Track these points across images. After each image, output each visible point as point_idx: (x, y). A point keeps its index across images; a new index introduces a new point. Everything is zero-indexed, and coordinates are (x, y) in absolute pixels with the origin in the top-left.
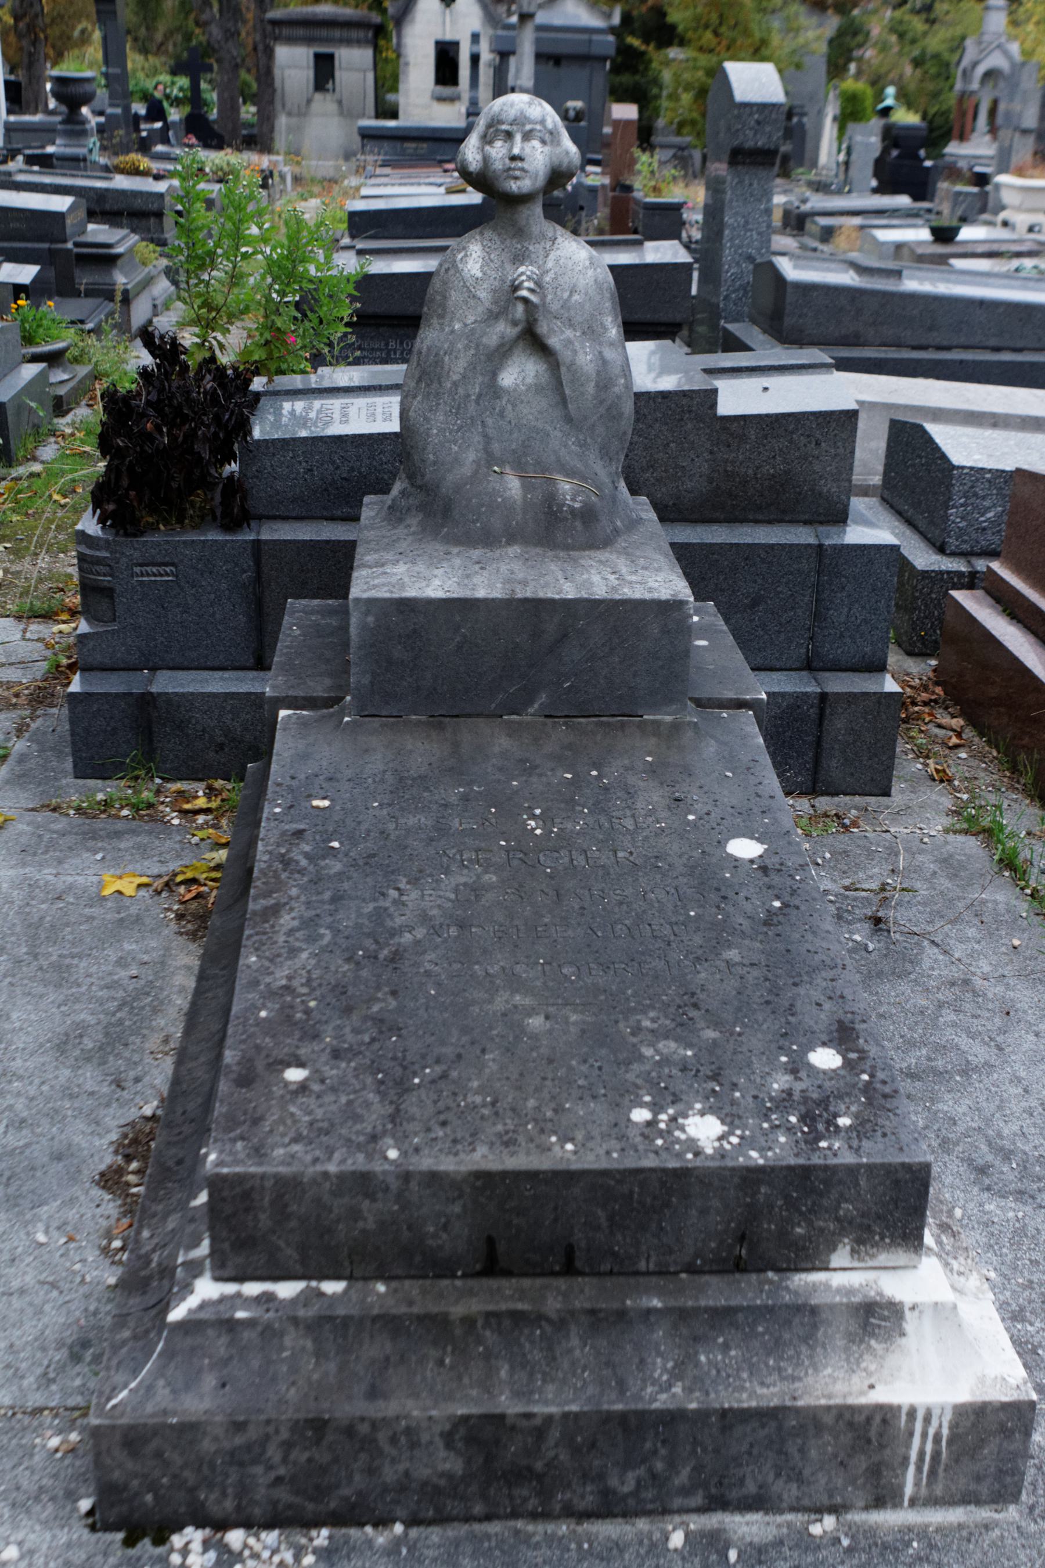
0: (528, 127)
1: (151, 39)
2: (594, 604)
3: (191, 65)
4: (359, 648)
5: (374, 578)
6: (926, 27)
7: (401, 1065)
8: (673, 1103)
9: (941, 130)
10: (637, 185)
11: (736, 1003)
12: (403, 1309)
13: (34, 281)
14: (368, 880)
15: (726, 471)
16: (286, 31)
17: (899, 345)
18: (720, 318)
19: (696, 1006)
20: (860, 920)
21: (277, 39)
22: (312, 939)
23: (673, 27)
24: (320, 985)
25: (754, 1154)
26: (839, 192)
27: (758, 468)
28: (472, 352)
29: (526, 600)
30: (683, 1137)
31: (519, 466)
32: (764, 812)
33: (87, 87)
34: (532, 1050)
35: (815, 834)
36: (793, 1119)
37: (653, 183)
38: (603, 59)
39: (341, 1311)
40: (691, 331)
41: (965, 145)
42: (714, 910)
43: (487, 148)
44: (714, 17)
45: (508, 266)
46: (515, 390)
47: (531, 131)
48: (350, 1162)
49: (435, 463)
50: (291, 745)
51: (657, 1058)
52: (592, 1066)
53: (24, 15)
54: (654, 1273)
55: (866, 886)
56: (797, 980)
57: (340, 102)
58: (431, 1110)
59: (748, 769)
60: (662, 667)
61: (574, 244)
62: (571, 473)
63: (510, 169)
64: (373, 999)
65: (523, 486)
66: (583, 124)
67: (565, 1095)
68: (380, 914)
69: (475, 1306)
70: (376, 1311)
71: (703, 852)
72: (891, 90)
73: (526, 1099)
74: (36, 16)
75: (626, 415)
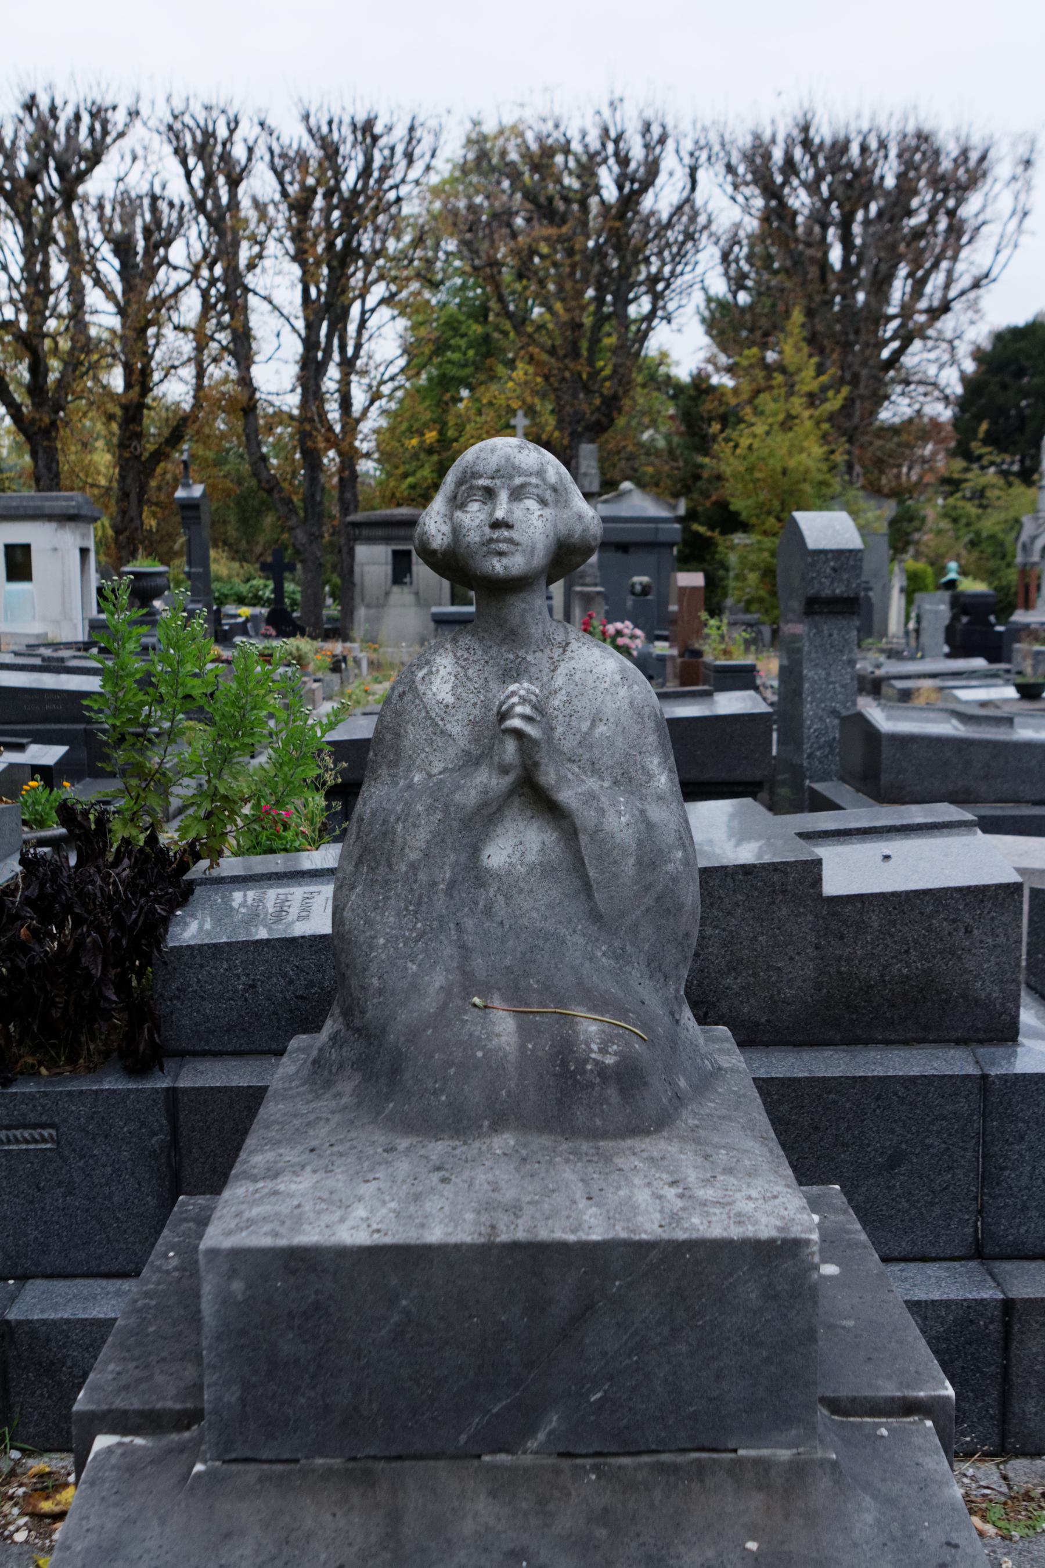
0: (518, 481)
1: (251, 551)
2: (639, 1249)
3: (276, 570)
4: (219, 1338)
5: (254, 1203)
6: (980, 511)
9: (1004, 603)
10: (706, 648)
13: (57, 764)
15: (839, 972)
16: (365, 532)
17: (1017, 801)
18: (804, 778)
21: (357, 539)
23: (737, 514)
26: (912, 658)
27: (885, 967)
28: (439, 816)
29: (515, 1246)
31: (516, 996)
33: (160, 581)
37: (723, 646)
38: (671, 545)
40: (772, 793)
41: (1031, 612)
43: (458, 514)
44: (776, 504)
45: (494, 685)
46: (509, 873)
47: (523, 486)
49: (381, 992)
50: (94, 1521)
53: (125, 529)
57: (417, 594)
61: (597, 651)
62: (599, 1004)
63: (491, 540)
65: (520, 1028)
66: (650, 597)
72: (953, 565)
74: (136, 529)
75: (688, 907)
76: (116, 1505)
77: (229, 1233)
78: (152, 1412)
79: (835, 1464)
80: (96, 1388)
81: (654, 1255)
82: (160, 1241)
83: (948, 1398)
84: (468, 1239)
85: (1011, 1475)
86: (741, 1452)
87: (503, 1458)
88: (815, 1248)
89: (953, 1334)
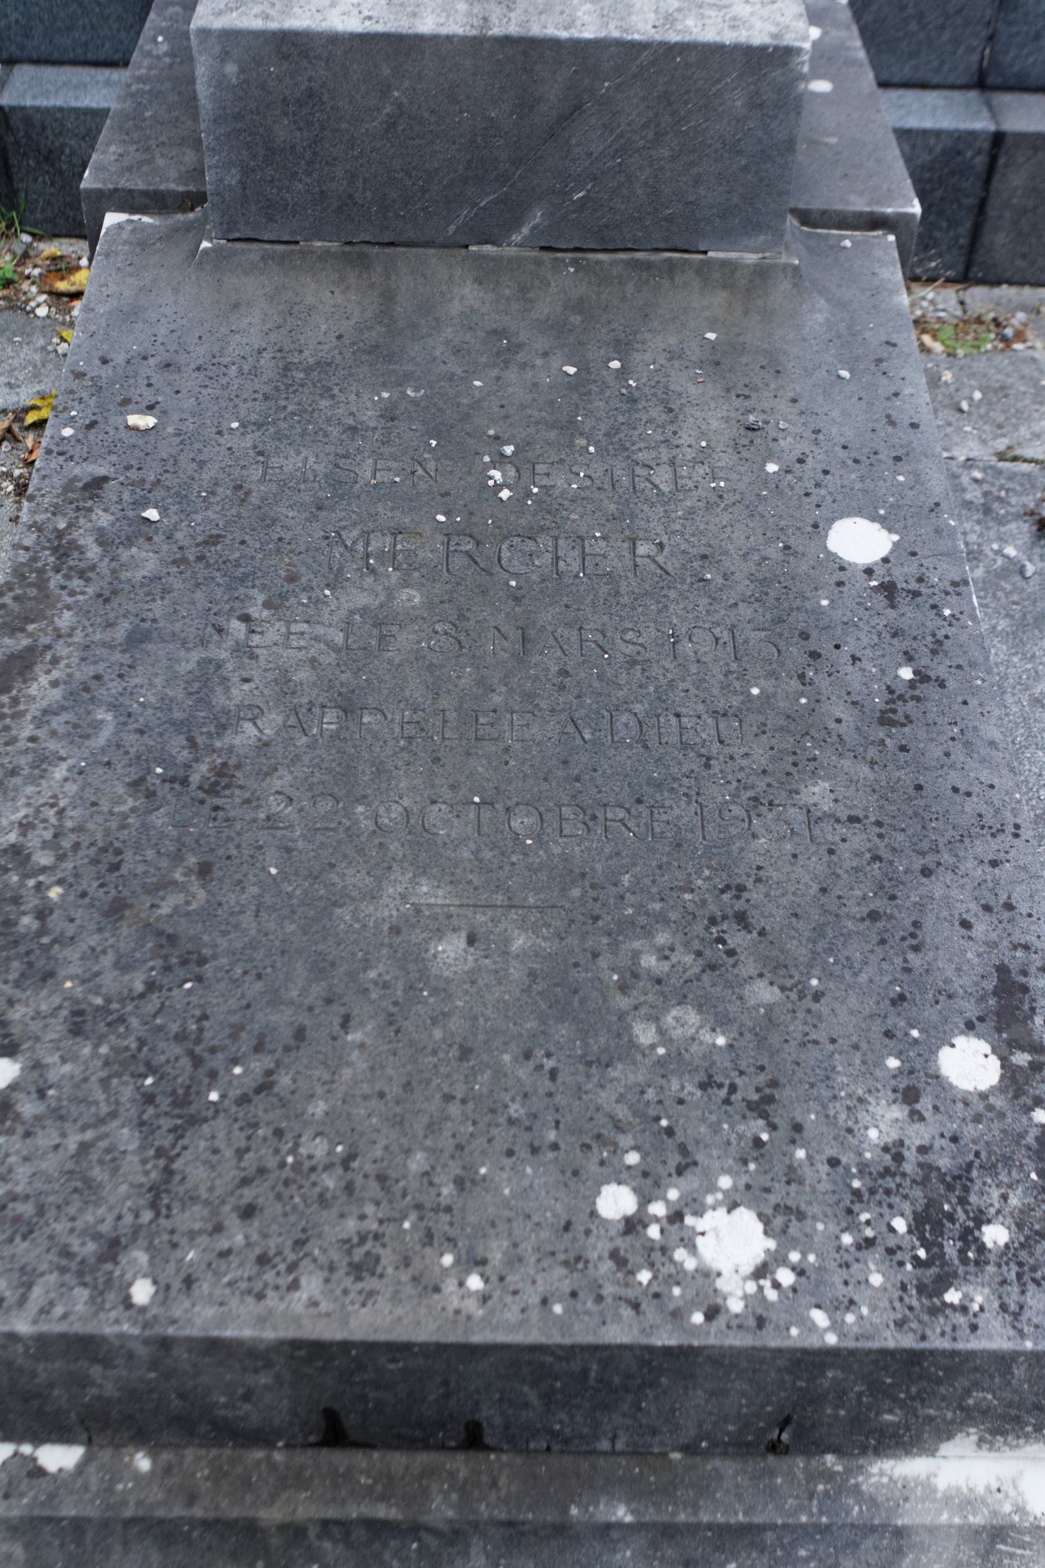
2: (633, 49)
7: (191, 1053)
8: (680, 1171)
11: (815, 915)
12: (178, 1511)
14: (199, 595)
19: (741, 919)
20: (1017, 517)
22: (80, 733)
24: (76, 846)
25: (820, 1318)
29: (507, 40)
30: (690, 1264)
32: (897, 459)
34: (435, 1021)
35: (960, 352)
36: (900, 1225)
39: (69, 1510)
42: (795, 684)
48: (59, 1310)
50: (112, 289)
51: (661, 1051)
52: (540, 1067)
54: (622, 1453)
55: (1028, 453)
56: (930, 860)
58: (230, 1173)
59: (879, 361)
60: (745, 169)
64: (167, 884)
67: (480, 1142)
68: (209, 674)
69: (305, 1507)
70: (128, 1513)
71: (787, 547)
73: (408, 1152)
76: (131, 275)
77: (219, 13)
78: (155, 192)
79: (796, 269)
80: (100, 168)
81: (645, 56)
82: (147, 25)
83: (913, 215)
84: (460, 31)
85: (968, 300)
86: (711, 254)
87: (488, 248)
88: (806, 58)
89: (936, 164)
